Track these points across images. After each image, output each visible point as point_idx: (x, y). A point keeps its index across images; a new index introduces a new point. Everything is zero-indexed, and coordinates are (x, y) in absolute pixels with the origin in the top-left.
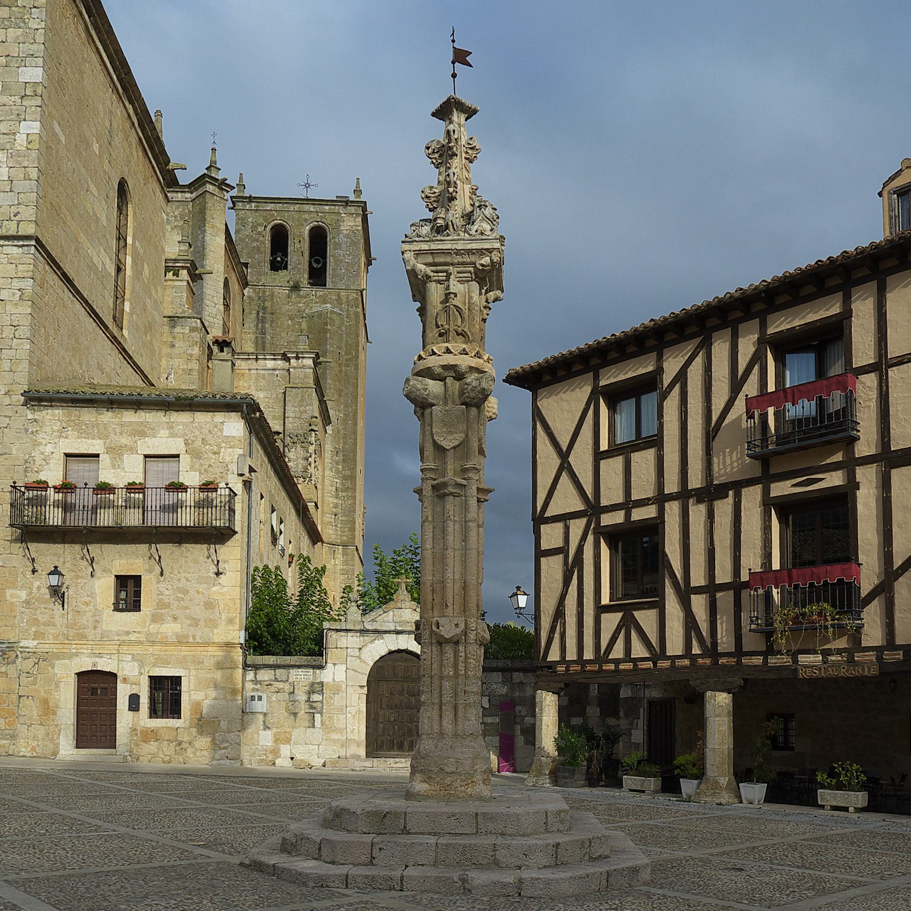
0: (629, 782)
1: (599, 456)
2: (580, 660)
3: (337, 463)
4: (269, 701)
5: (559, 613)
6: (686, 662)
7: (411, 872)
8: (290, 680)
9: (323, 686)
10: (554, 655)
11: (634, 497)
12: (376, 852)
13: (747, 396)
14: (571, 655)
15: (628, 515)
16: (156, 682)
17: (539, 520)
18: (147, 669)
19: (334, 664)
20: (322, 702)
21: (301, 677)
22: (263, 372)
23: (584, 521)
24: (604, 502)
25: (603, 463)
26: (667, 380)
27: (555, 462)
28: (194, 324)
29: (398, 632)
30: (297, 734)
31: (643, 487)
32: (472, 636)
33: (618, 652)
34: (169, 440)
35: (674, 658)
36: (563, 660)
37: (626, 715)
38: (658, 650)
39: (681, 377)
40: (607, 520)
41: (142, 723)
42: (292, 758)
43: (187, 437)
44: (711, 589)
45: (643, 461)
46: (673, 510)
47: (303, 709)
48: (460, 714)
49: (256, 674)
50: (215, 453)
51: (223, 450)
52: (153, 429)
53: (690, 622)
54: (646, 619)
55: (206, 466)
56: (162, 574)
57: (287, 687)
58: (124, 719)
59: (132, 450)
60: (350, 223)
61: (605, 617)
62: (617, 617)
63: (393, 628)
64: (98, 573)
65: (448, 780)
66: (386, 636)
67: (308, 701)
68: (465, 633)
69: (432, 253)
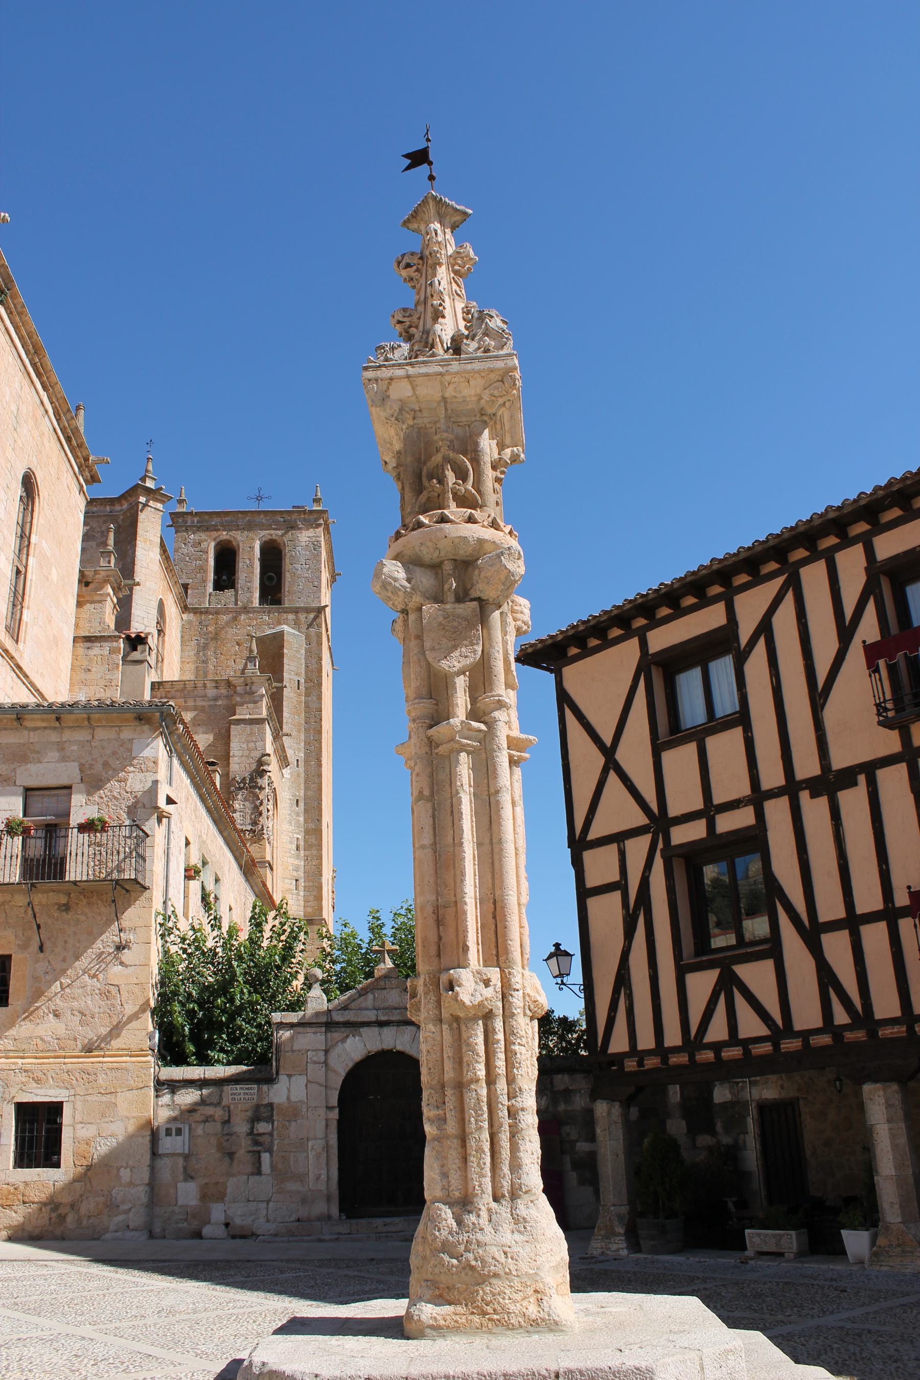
0: (757, 1240)
2: (661, 1050)
5: (623, 979)
9: (272, 1109)
10: (619, 1044)
11: (717, 799)
13: (864, 642)
14: (646, 1041)
15: (711, 826)
17: (579, 844)
19: (289, 1076)
20: (271, 1134)
23: (646, 839)
26: (744, 636)
27: (600, 760)
29: (381, 1024)
31: (730, 782)
33: (718, 1031)
34: (58, 765)
35: (806, 1035)
36: (633, 1049)
38: (779, 1022)
39: (765, 628)
40: (681, 835)
43: (83, 761)
44: (853, 922)
45: (726, 748)
46: (777, 812)
47: (244, 1146)
52: (38, 752)
53: (826, 977)
54: (757, 976)
56: (41, 948)
57: (218, 1113)
63: (373, 1019)
66: (364, 1030)
67: (251, 1133)
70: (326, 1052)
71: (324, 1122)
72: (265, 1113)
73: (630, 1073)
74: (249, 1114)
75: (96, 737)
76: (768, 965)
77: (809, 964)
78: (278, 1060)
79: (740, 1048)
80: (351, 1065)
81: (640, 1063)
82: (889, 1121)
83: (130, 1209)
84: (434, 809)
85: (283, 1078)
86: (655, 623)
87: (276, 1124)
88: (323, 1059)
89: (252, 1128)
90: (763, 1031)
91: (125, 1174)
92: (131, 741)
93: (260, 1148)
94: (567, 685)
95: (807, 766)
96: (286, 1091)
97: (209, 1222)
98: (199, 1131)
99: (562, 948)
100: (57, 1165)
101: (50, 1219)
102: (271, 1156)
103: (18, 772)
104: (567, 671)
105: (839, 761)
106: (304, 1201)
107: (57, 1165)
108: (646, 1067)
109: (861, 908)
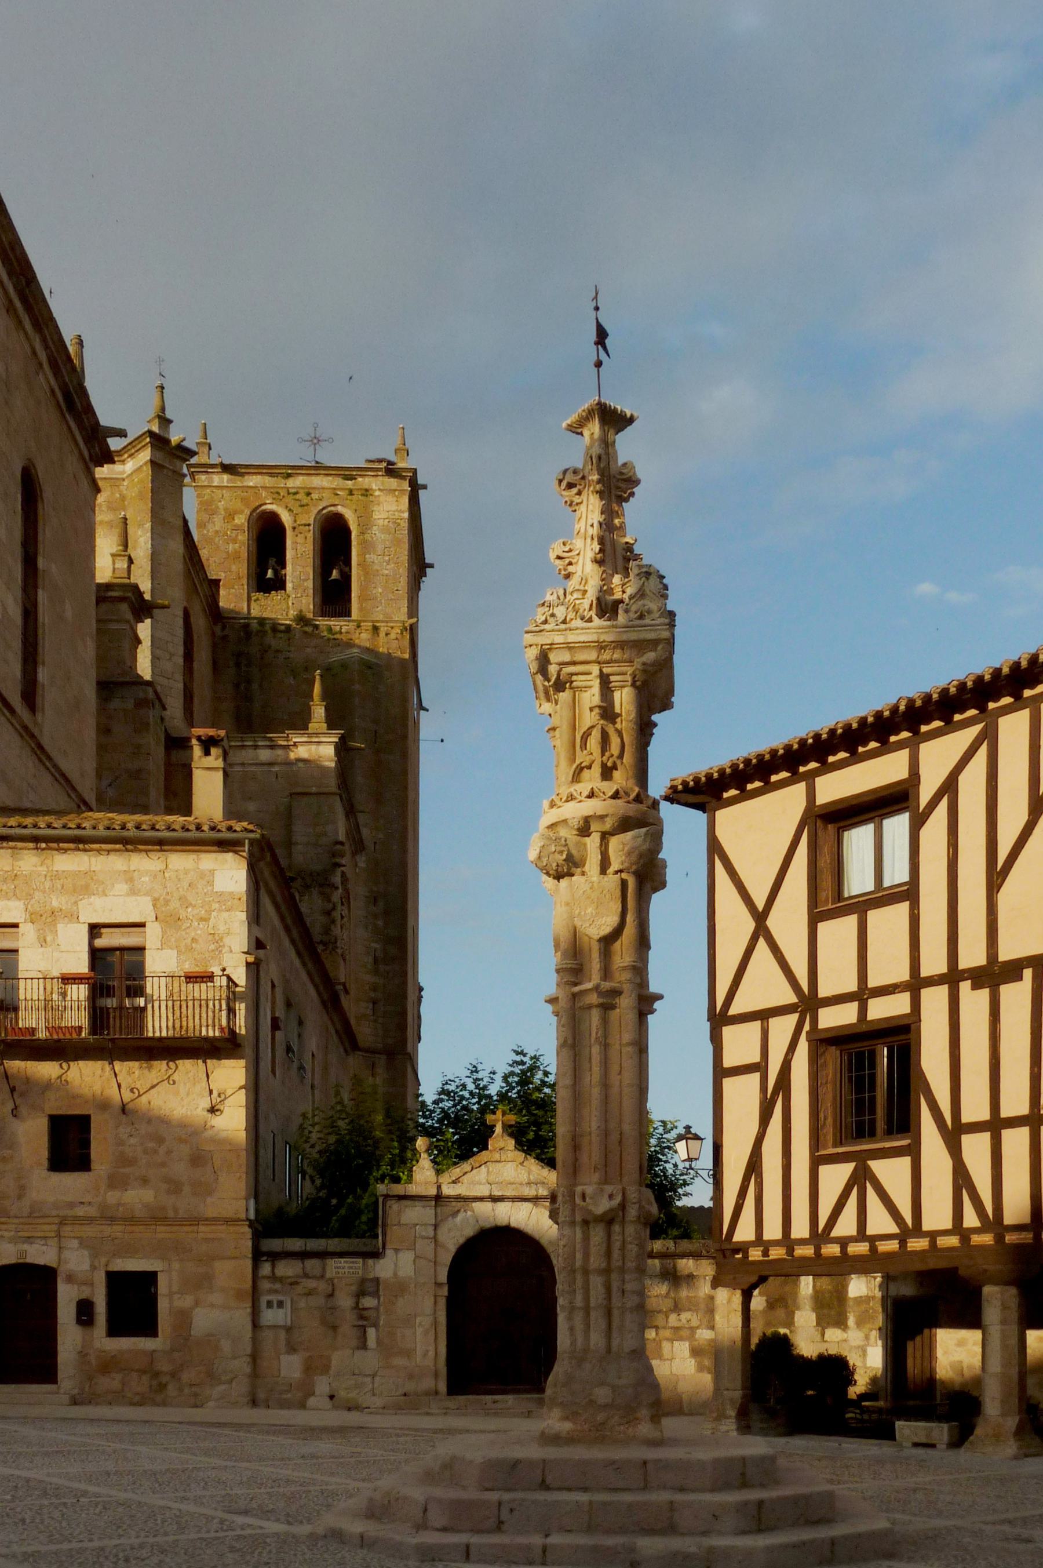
1: (816, 917)
2: (787, 1240)
3: (376, 916)
4: (294, 1310)
5: (754, 1166)
6: (953, 1241)
7: (555, 1539)
8: (328, 1275)
10: (745, 1233)
12: (505, 1515)
14: (773, 1231)
15: (863, 1011)
16: (117, 1281)
17: (719, 1019)
18: (103, 1260)
19: (397, 1250)
20: (377, 1309)
21: (344, 1270)
22: (253, 768)
23: (794, 1018)
24: (823, 992)
25: (821, 926)
26: (925, 795)
28: (141, 695)
30: (337, 1359)
31: (889, 965)
32: (632, 1212)
33: (846, 1226)
35: (933, 1235)
37: (859, 1324)
38: (909, 1221)
39: (950, 787)
40: (831, 1018)
41: (97, 1344)
42: (332, 1397)
43: (156, 895)
44: (996, 1125)
45: (889, 924)
46: (935, 999)
47: (348, 1320)
48: (616, 1323)
49: (273, 1267)
50: (202, 919)
51: (214, 914)
53: (962, 1179)
54: (894, 1173)
55: (189, 940)
57: (322, 1286)
58: (69, 1337)
59: (73, 917)
60: (389, 506)
61: (826, 1171)
62: (846, 1170)
63: (487, 1193)
64: (23, 1110)
65: (600, 1417)
67: (357, 1307)
68: (623, 1206)
69: (570, 648)
70: (436, 1226)
71: (432, 1299)
72: (370, 1287)
73: (754, 1263)
74: (354, 1288)
75: (170, 866)
76: (906, 1162)
77: (948, 1163)
78: (384, 1235)
79: (867, 1244)
80: (462, 1240)
81: (766, 1253)
82: (1004, 1322)
83: (232, 1379)
84: (575, 1055)
85: (389, 1252)
86: (826, 768)
87: (382, 1299)
88: (431, 1234)
89: (357, 1303)
90: (894, 1229)
91: (226, 1346)
92: (212, 872)
93: (365, 1323)
94: (719, 833)
95: (973, 954)
96: (393, 1266)
97: (313, 1394)
98: (302, 1304)
99: (693, 1131)
100: (155, 1334)
101: (151, 1386)
102: (377, 1330)
103: (80, 906)
104: (721, 815)
105: (1006, 953)
106: (411, 1377)
107: (155, 1334)
108: (771, 1257)
109: (1007, 1111)
